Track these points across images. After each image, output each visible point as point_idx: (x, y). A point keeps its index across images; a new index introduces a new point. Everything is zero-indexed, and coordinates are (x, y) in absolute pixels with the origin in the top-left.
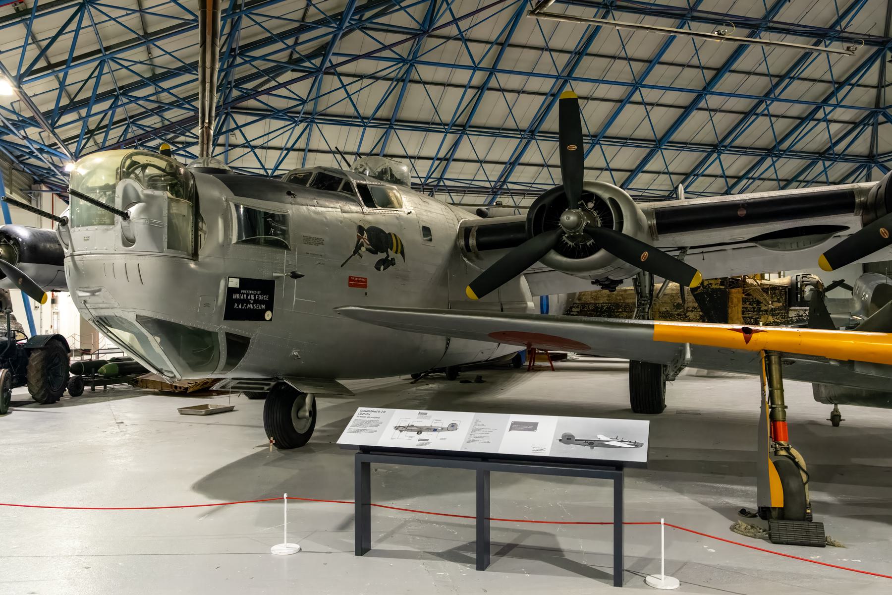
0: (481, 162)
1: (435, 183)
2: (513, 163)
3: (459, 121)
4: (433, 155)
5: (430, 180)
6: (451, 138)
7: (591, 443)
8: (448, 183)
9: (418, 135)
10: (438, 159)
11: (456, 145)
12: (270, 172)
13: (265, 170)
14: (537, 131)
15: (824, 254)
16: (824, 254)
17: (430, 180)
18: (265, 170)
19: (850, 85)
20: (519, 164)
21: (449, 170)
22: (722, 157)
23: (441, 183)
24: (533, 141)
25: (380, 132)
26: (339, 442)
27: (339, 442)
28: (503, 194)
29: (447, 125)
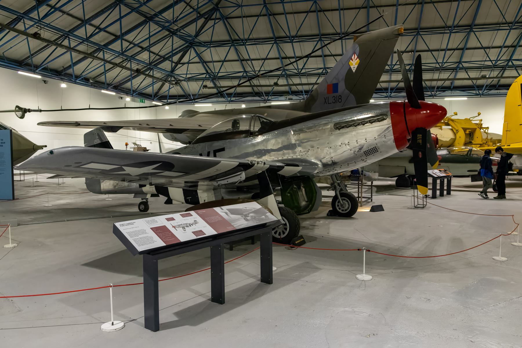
0: (484, 48)
10: (505, 47)
23: (510, 64)
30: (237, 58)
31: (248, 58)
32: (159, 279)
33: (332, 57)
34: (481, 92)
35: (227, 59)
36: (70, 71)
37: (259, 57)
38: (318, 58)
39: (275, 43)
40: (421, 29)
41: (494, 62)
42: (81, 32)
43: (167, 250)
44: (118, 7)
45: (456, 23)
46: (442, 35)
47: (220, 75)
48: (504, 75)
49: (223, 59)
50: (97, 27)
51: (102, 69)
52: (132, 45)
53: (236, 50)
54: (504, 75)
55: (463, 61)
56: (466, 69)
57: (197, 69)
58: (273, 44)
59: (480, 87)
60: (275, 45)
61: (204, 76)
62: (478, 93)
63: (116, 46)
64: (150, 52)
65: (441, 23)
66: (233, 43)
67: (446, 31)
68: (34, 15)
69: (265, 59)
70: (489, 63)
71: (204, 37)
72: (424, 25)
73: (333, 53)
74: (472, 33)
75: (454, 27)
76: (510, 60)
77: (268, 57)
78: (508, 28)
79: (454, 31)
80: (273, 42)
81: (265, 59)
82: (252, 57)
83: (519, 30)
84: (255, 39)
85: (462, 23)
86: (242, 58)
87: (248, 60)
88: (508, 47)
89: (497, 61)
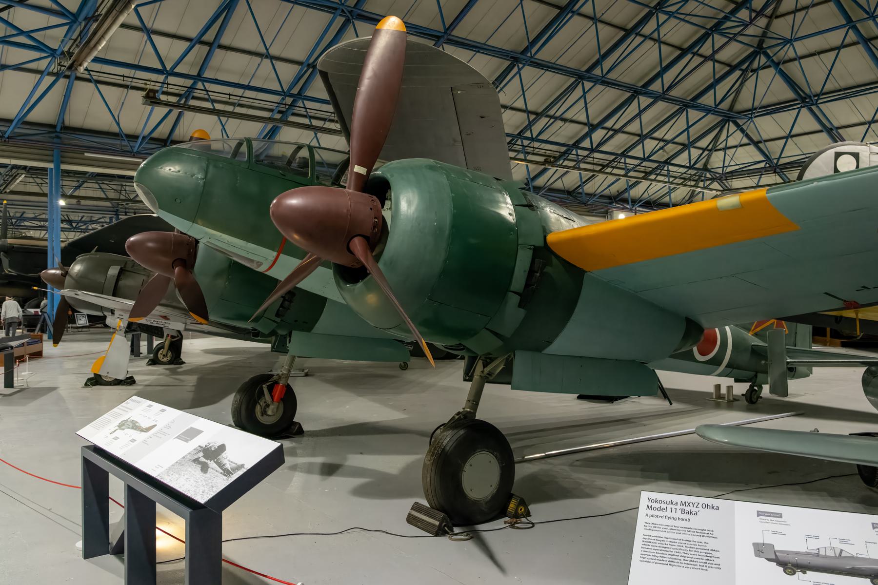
7: (707, 506)
15: (754, 544)
19: (547, 116)
32: (183, 565)
36: (626, 195)
42: (637, 152)
44: (685, 112)
47: (782, 161)
50: (609, 129)
51: (666, 190)
52: (552, 120)
57: (748, 155)
61: (762, 165)
63: (683, 159)
64: (267, 50)
68: (586, 144)
71: (745, 102)
84: (840, 90)
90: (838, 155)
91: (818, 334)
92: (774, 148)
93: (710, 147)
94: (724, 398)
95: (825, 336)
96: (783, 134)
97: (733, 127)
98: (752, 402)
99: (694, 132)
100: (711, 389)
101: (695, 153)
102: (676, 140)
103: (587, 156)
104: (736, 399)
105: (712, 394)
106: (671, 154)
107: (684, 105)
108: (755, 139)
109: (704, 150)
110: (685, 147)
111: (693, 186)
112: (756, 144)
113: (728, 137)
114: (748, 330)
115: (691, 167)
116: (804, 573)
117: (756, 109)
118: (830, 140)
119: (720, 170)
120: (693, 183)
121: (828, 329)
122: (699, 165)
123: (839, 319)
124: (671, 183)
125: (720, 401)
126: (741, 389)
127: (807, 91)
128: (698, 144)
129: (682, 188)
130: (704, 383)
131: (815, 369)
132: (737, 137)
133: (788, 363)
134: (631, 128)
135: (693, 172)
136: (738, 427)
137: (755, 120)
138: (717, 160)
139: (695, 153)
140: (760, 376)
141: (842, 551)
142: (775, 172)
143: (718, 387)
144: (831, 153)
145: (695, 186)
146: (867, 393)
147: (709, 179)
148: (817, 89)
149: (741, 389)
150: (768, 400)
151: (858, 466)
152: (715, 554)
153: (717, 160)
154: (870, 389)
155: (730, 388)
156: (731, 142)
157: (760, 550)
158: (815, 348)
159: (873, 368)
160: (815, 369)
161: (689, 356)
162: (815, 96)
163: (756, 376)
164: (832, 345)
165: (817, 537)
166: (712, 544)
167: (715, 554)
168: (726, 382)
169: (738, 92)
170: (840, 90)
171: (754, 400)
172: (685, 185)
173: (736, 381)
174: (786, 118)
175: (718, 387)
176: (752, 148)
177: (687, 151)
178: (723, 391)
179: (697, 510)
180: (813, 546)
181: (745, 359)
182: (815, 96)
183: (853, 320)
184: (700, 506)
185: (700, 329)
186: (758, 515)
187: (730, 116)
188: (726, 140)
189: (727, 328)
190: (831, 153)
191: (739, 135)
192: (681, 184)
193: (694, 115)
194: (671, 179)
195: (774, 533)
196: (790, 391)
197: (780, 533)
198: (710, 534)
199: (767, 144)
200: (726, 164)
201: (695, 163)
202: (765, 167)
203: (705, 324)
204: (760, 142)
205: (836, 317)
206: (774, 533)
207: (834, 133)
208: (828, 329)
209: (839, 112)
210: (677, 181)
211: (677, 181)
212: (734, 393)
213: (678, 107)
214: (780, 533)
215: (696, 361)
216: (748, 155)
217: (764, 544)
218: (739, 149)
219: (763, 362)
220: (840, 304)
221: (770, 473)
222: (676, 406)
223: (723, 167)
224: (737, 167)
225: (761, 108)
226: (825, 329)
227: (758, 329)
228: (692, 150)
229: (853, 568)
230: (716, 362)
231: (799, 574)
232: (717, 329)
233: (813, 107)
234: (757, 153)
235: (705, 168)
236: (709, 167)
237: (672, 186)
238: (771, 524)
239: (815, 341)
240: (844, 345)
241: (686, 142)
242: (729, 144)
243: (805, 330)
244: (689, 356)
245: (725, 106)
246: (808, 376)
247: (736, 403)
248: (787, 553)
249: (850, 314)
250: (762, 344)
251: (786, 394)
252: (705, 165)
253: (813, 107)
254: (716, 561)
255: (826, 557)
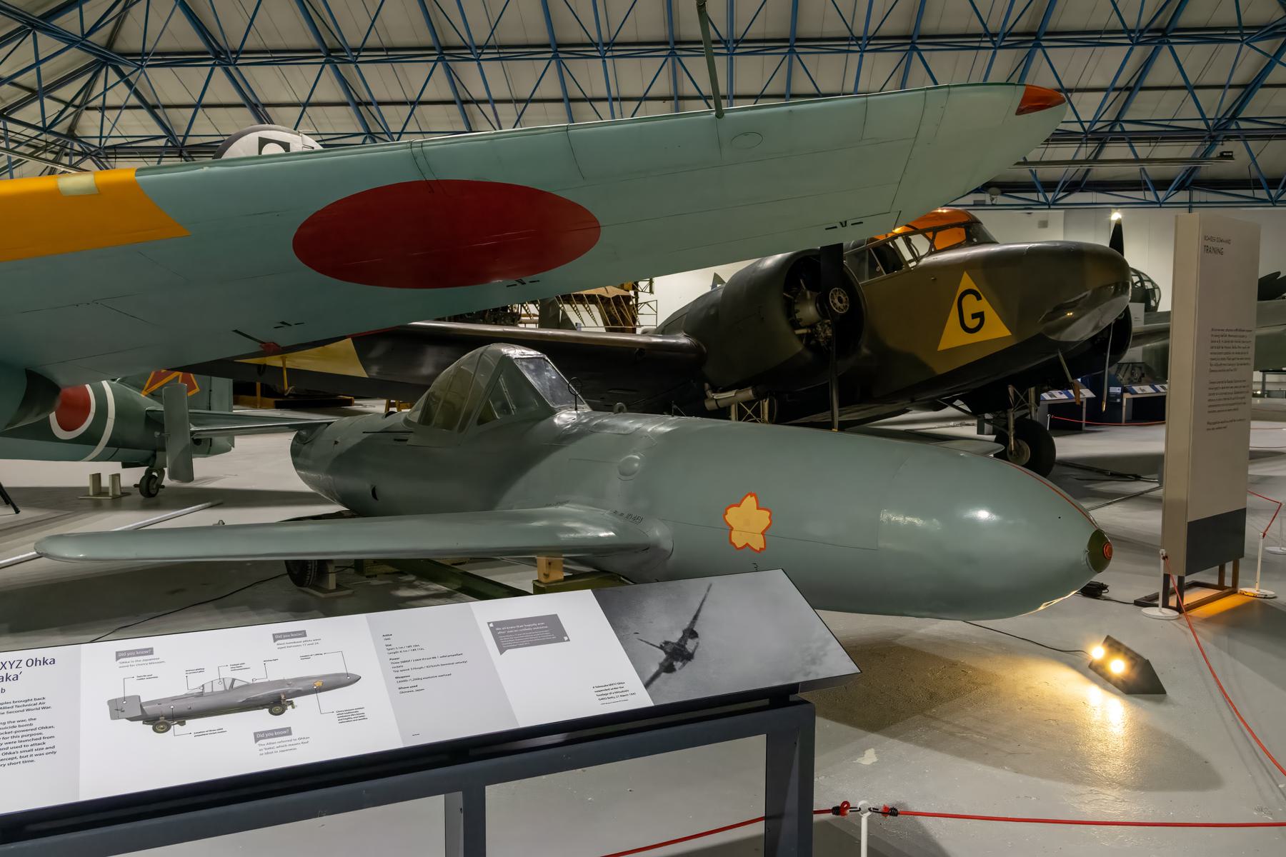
1: (1107, 129)
2: (1248, 89)
3: (1022, 25)
4: (1223, 81)
5: (1098, 125)
6: (1140, 52)
7: (35, 662)
8: (1128, 127)
9: (1083, 54)
10: (1115, 89)
11: (1147, 65)
12: (1087, 125)
13: (1081, 123)
14: (1171, 28)
15: (110, 702)
16: (110, 702)
17: (1098, 125)
18: (1081, 123)
20: (88, 109)
21: (1133, 106)
22: (327, 66)
23: (1118, 129)
24: (1039, 51)
25: (1020, 54)
26: (942, 347)
27: (942, 347)
28: (1228, 138)
29: (996, 35)
30: (450, 95)
31: (485, 96)
33: (588, 104)
34: (1050, 196)
35: (313, 99)
37: (401, 97)
38: (547, 105)
39: (441, 59)
40: (920, 37)
41: (1087, 125)
43: (1247, 732)
44: (31, 36)
45: (870, 34)
46: (974, 52)
47: (190, 141)
48: (1102, 157)
49: (304, 99)
53: (449, 71)
54: (1102, 157)
55: (1125, 118)
56: (1246, 136)
57: (137, 125)
58: (550, 59)
59: (1049, 186)
60: (439, 64)
61: (162, 142)
62: (1042, 199)
63: (31, 113)
65: (841, 30)
66: (328, 55)
67: (852, 48)
69: (527, 101)
70: (1076, 127)
72: (929, 25)
73: (589, 95)
74: (1166, 48)
75: (869, 39)
76: (1118, 120)
77: (650, 94)
78: (1128, 41)
79: (869, 48)
80: (550, 55)
81: (527, 101)
82: (495, 95)
83: (1014, 51)
85: (887, 28)
86: (464, 96)
87: (371, 104)
88: (1120, 89)
89: (1093, 123)
90: (263, 142)
91: (242, 392)
92: (179, 119)
93: (77, 102)
94: (106, 494)
95: (255, 394)
96: (192, 102)
97: (113, 77)
98: (150, 494)
99: (50, 71)
100: (87, 483)
101: (52, 108)
102: (17, 80)
103: (35, 138)
104: (126, 493)
105: (87, 488)
106: (11, 102)
107: (32, 25)
108: (150, 101)
109: (68, 105)
110: (36, 94)
111: (53, 162)
112: (152, 109)
113: (106, 90)
114: (140, 388)
115: (45, 130)
116: (182, 724)
117: (148, 54)
118: (254, 120)
119: (96, 142)
120: (51, 157)
121: (258, 385)
122: (61, 128)
123: (262, 369)
124: (12, 151)
125: (100, 497)
126: (132, 477)
127: (222, 42)
128: (59, 93)
129: (32, 162)
130: (74, 473)
131: (238, 440)
132: (119, 94)
133: (193, 433)
134: (25, 79)
135: (51, 138)
136: (137, 532)
137: (147, 70)
138: (90, 124)
139: (52, 108)
140: (159, 454)
141: (234, 680)
142: (180, 156)
143: (97, 478)
144: (253, 138)
145: (55, 161)
146: (297, 466)
147: (79, 154)
148: (236, 44)
149: (132, 477)
150: (172, 489)
151: (286, 562)
152: (46, 733)
153: (90, 124)
154: (299, 460)
155: (115, 478)
156: (112, 99)
157: (118, 709)
158: (238, 411)
159: (304, 433)
160: (238, 440)
161: (43, 432)
162: (233, 52)
163: (154, 456)
164: (263, 406)
165: (201, 670)
166: (41, 718)
167: (46, 733)
168: (108, 469)
169: (120, 20)
170: (266, 52)
171: (153, 492)
172: (37, 158)
173: (125, 466)
174: (195, 76)
175: (97, 478)
176: (144, 113)
177: (37, 103)
178: (106, 482)
179: (17, 671)
180: (195, 684)
181: (136, 432)
182: (233, 52)
183: (281, 369)
184: (23, 664)
185: (54, 389)
186: (118, 659)
187: (107, 58)
188: (104, 94)
189: (105, 383)
190: (253, 138)
191: (123, 90)
192: (31, 155)
193: (48, 44)
194: (12, 145)
195: (141, 678)
196: (196, 476)
197: (150, 677)
198: (39, 704)
199: (167, 111)
200: (105, 133)
201: (54, 123)
202: (166, 146)
203: (62, 380)
204: (157, 107)
205: (259, 366)
206: (141, 678)
207: (261, 111)
208: (258, 385)
209: (267, 82)
210: (21, 149)
211: (21, 149)
212: (123, 484)
213: (18, 25)
214: (150, 677)
215: (55, 439)
216: (137, 125)
217: (124, 699)
218: (125, 112)
219: (157, 434)
220: (256, 347)
221: (174, 592)
222: (26, 514)
223: (101, 137)
224: (130, 140)
225: (155, 54)
226: (254, 385)
227: (156, 387)
228: (46, 101)
229: (248, 700)
230: (90, 439)
231: (176, 728)
232: (88, 386)
233: (231, 68)
234: (153, 122)
235: (71, 134)
236: (77, 133)
237: (15, 158)
238: (137, 667)
239: (236, 402)
240: (278, 406)
241: (36, 87)
242: (109, 102)
243: (223, 386)
244: (43, 432)
245: (99, 38)
246: (228, 450)
247: (125, 499)
248: (159, 702)
249: (274, 361)
250: (161, 408)
251: (190, 478)
252: (72, 129)
253: (231, 68)
254: (49, 743)
255: (213, 694)
